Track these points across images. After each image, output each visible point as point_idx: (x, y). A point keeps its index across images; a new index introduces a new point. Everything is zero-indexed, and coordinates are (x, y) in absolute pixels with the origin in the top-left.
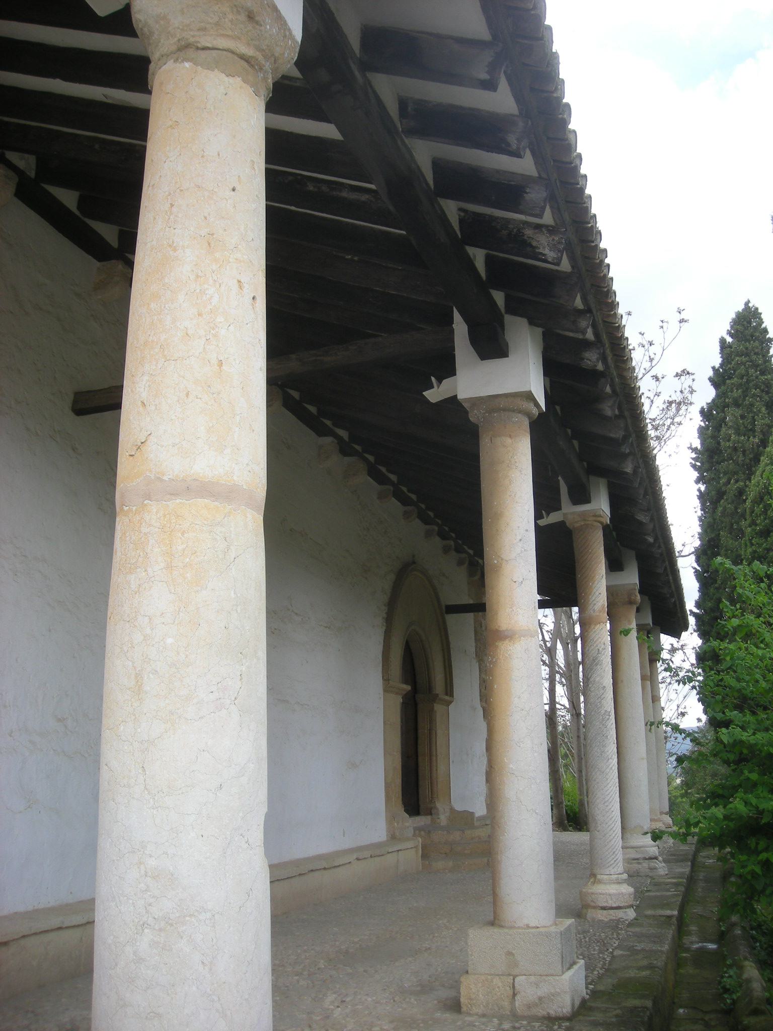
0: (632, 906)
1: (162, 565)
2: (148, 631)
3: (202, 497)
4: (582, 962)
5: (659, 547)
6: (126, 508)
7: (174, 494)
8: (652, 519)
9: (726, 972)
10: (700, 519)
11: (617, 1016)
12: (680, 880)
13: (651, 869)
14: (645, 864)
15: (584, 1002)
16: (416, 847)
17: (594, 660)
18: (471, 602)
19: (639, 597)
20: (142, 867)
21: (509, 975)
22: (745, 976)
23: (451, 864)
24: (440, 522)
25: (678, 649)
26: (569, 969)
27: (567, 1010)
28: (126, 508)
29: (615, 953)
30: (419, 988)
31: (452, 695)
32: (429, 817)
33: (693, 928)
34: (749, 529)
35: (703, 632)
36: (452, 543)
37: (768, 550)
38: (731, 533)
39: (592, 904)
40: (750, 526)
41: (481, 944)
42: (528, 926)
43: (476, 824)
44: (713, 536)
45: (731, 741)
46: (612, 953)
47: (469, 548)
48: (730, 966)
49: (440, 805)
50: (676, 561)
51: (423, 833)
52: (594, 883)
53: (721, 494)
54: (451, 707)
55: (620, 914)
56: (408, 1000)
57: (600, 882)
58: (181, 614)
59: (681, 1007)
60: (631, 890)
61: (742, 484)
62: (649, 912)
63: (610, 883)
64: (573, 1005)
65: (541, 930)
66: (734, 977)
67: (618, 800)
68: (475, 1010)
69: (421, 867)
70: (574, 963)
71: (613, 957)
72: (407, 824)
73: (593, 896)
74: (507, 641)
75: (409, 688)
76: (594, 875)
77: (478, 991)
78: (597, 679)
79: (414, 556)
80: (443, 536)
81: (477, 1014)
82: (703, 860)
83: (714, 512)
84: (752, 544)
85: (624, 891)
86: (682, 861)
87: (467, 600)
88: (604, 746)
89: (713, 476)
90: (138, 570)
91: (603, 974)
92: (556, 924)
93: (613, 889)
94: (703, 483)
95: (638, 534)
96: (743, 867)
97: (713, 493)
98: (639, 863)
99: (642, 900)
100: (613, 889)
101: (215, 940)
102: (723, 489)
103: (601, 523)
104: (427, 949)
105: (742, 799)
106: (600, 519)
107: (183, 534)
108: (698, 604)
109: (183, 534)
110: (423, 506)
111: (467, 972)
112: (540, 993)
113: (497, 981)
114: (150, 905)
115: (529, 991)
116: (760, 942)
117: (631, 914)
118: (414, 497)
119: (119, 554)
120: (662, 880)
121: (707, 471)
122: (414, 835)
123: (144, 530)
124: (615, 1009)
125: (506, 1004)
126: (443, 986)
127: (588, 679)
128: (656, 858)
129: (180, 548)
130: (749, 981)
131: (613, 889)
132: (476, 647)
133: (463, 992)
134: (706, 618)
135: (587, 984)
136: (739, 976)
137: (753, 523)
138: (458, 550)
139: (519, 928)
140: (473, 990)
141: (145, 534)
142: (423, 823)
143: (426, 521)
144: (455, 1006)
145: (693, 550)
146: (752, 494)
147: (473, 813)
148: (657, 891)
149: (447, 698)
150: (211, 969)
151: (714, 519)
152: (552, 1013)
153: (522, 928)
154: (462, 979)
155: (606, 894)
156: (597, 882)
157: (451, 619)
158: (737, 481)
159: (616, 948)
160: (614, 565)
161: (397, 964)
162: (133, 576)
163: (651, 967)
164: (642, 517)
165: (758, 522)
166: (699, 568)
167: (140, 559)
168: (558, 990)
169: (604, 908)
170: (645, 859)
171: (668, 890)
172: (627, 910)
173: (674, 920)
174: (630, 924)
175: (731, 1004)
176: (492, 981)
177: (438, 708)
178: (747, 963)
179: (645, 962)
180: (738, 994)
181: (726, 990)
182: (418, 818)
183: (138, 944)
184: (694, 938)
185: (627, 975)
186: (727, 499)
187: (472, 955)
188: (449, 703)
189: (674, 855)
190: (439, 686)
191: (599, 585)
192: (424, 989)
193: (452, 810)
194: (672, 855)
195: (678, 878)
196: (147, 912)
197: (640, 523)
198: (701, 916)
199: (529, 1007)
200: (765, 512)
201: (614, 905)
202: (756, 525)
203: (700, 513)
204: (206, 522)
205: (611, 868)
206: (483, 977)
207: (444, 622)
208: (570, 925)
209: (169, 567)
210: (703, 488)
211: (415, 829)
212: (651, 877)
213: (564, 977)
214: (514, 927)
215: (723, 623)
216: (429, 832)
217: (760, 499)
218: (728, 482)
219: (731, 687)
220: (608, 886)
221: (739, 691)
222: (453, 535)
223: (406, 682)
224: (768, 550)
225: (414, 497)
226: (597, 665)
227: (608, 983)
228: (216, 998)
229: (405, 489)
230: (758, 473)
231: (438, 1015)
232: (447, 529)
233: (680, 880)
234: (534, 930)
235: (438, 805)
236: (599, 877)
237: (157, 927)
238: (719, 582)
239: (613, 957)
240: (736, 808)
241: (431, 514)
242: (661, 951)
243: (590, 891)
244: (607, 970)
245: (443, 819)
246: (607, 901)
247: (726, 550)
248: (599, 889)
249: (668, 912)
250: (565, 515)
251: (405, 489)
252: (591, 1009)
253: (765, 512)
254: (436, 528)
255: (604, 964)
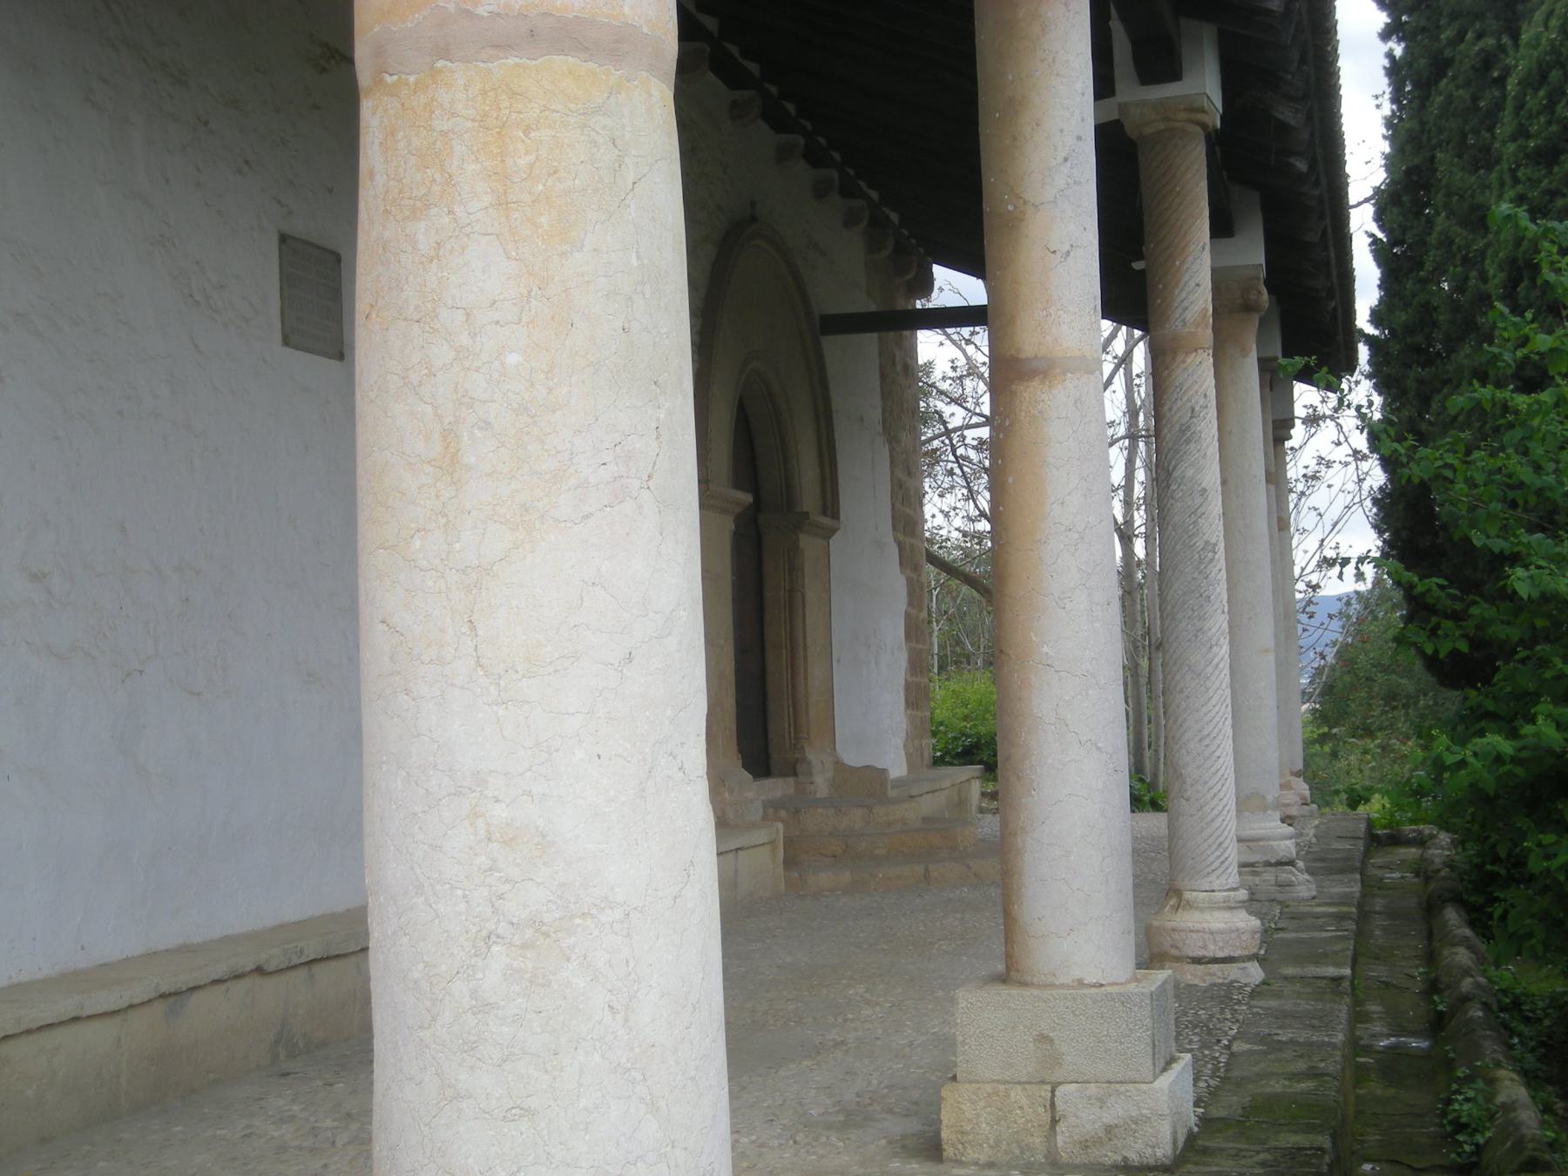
0: (1254, 957)
1: (487, 199)
2: (465, 340)
3: (562, 51)
4: (1188, 1057)
5: (1317, 183)
6: (389, 79)
7: (503, 46)
8: (1309, 119)
9: (1458, 1092)
10: (1389, 123)
11: (1263, 1164)
12: (1345, 909)
13: (1281, 885)
14: (1269, 876)
15: (1191, 1138)
16: (772, 842)
17: (1183, 432)
18: (873, 308)
19: (1265, 295)
20: (480, 823)
21: (1043, 1082)
22: (1501, 1098)
23: (846, 877)
24: (808, 125)
25: (1324, 417)
26: (1164, 1070)
27: (1163, 1150)
28: (389, 79)
29: (1235, 1048)
30: (841, 1117)
31: (835, 515)
32: (791, 780)
33: (1374, 1008)
34: (1511, 147)
35: (1384, 380)
36: (835, 174)
37: (1553, 194)
38: (1460, 156)
39: (1174, 952)
40: (1513, 138)
41: (984, 1022)
42: (1081, 983)
43: (892, 793)
44: (1417, 161)
45: (1535, 594)
46: (1228, 1047)
47: (870, 187)
48: (1469, 1079)
49: (814, 755)
50: (1348, 218)
51: (783, 813)
52: (1176, 908)
53: (1440, 66)
54: (835, 541)
55: (1233, 972)
56: (823, 1139)
57: (1190, 905)
58: (534, 303)
59: (1367, 1161)
60: (1255, 923)
61: (1490, 41)
62: (1290, 971)
63: (1211, 909)
64: (1175, 1142)
65: (1109, 989)
66: (1481, 1099)
67: (1230, 732)
68: (971, 1154)
69: (783, 887)
70: (1170, 1062)
71: (1232, 1055)
72: (750, 795)
73: (1176, 936)
74: (1035, 383)
75: (747, 498)
76: (1178, 893)
77: (978, 1116)
78: (1190, 473)
79: (753, 203)
80: (814, 158)
81: (977, 1164)
82: (1379, 873)
83: (1423, 106)
84: (1516, 181)
85: (1241, 925)
86: (1342, 871)
87: (862, 303)
88: (1202, 618)
89: (1423, 23)
90: (434, 211)
91: (1217, 1088)
92: (1137, 980)
93: (1218, 921)
94: (1400, 40)
95: (1274, 159)
96: (1548, 857)
97: (1423, 62)
98: (1255, 874)
99: (1270, 951)
100: (1219, 921)
101: (632, 964)
102: (1448, 53)
103: (1204, 126)
104: (837, 1045)
105: (1549, 716)
106: (1199, 117)
107: (527, 131)
108: (1377, 317)
109: (527, 131)
110: (773, 89)
111: (954, 1078)
112: (1108, 1118)
113: (1018, 1095)
114: (501, 897)
115: (1083, 1114)
116: (1520, 1035)
117: (1255, 974)
118: (754, 68)
119: (380, 179)
120: (1306, 909)
121: (1410, 12)
122: (765, 817)
123: (441, 124)
124: (1258, 1152)
125: (1037, 1140)
126: (890, 1111)
127: (1169, 474)
128: (1291, 863)
129: (522, 162)
130: (1508, 1108)
131: (1218, 921)
132: (884, 410)
133: (947, 1117)
134: (1395, 348)
135: (1196, 1105)
136: (1490, 1098)
137: (1521, 133)
138: (847, 191)
139: (1062, 986)
140: (967, 1114)
141: (444, 133)
142: (779, 794)
143: (779, 123)
144: (931, 1148)
145: (1370, 193)
146: (1521, 63)
147: (884, 771)
148: (1296, 930)
149: (826, 521)
150: (626, 1021)
151: (1422, 123)
152: (1134, 1157)
153: (1068, 987)
154: (944, 1093)
155: (1203, 931)
156: (1182, 904)
157: (834, 347)
158: (1480, 36)
159: (1234, 1038)
160: (1222, 227)
161: (782, 1073)
162: (423, 224)
163: (1313, 1074)
164: (1287, 114)
165: (1534, 129)
166: (1380, 235)
167: (435, 188)
168: (1145, 1112)
169: (1197, 961)
170: (1268, 864)
171: (1322, 928)
172: (1248, 964)
173: (1346, 984)
174: (1256, 993)
175: (1472, 1153)
176: (1007, 1096)
177: (808, 544)
178: (1502, 1073)
179: (1301, 1066)
180: (1488, 1134)
181: (1460, 1127)
182: (768, 783)
183: (480, 975)
184: (1378, 1028)
185: (1268, 1090)
186: (1454, 78)
187: (963, 1043)
188: (828, 533)
189: (1323, 860)
190: (809, 500)
191: (1196, 269)
192: (853, 1118)
193: (838, 764)
194: (1316, 860)
195: (1338, 904)
196: (495, 911)
197: (1283, 128)
198: (1387, 984)
199: (1085, 1145)
200: (1550, 107)
201: (1220, 955)
202: (1528, 136)
203: (1387, 108)
204: (572, 106)
205: (1213, 877)
206: (989, 1088)
207: (820, 357)
208: (1165, 982)
209: (502, 203)
210: (1398, 51)
211: (767, 804)
212: (1280, 903)
213: (1157, 1084)
214: (1052, 985)
215: (1495, 350)
216: (797, 811)
217: (1539, 77)
218: (1461, 36)
219: (1521, 485)
220: (1207, 916)
221: (1540, 492)
222: (837, 156)
223: (737, 484)
224: (1553, 194)
225: (754, 68)
226: (1188, 442)
227: (1230, 1105)
228: (639, 1077)
229: (734, 50)
230: (1539, 16)
231: (895, 1165)
232: (822, 140)
233: (1345, 909)
234: (1094, 990)
235: (811, 755)
236: (1187, 895)
237: (517, 940)
238: (1428, 266)
239: (1232, 1055)
240: (1537, 734)
241: (791, 108)
242: (1330, 1044)
243: (1169, 925)
244: (1225, 1080)
245: (821, 784)
246: (1205, 947)
247: (1448, 195)
248: (1187, 920)
249: (1331, 971)
250: (1123, 107)
251: (734, 50)
252: (1205, 1151)
253: (1550, 107)
254: (801, 140)
255: (1216, 1069)
